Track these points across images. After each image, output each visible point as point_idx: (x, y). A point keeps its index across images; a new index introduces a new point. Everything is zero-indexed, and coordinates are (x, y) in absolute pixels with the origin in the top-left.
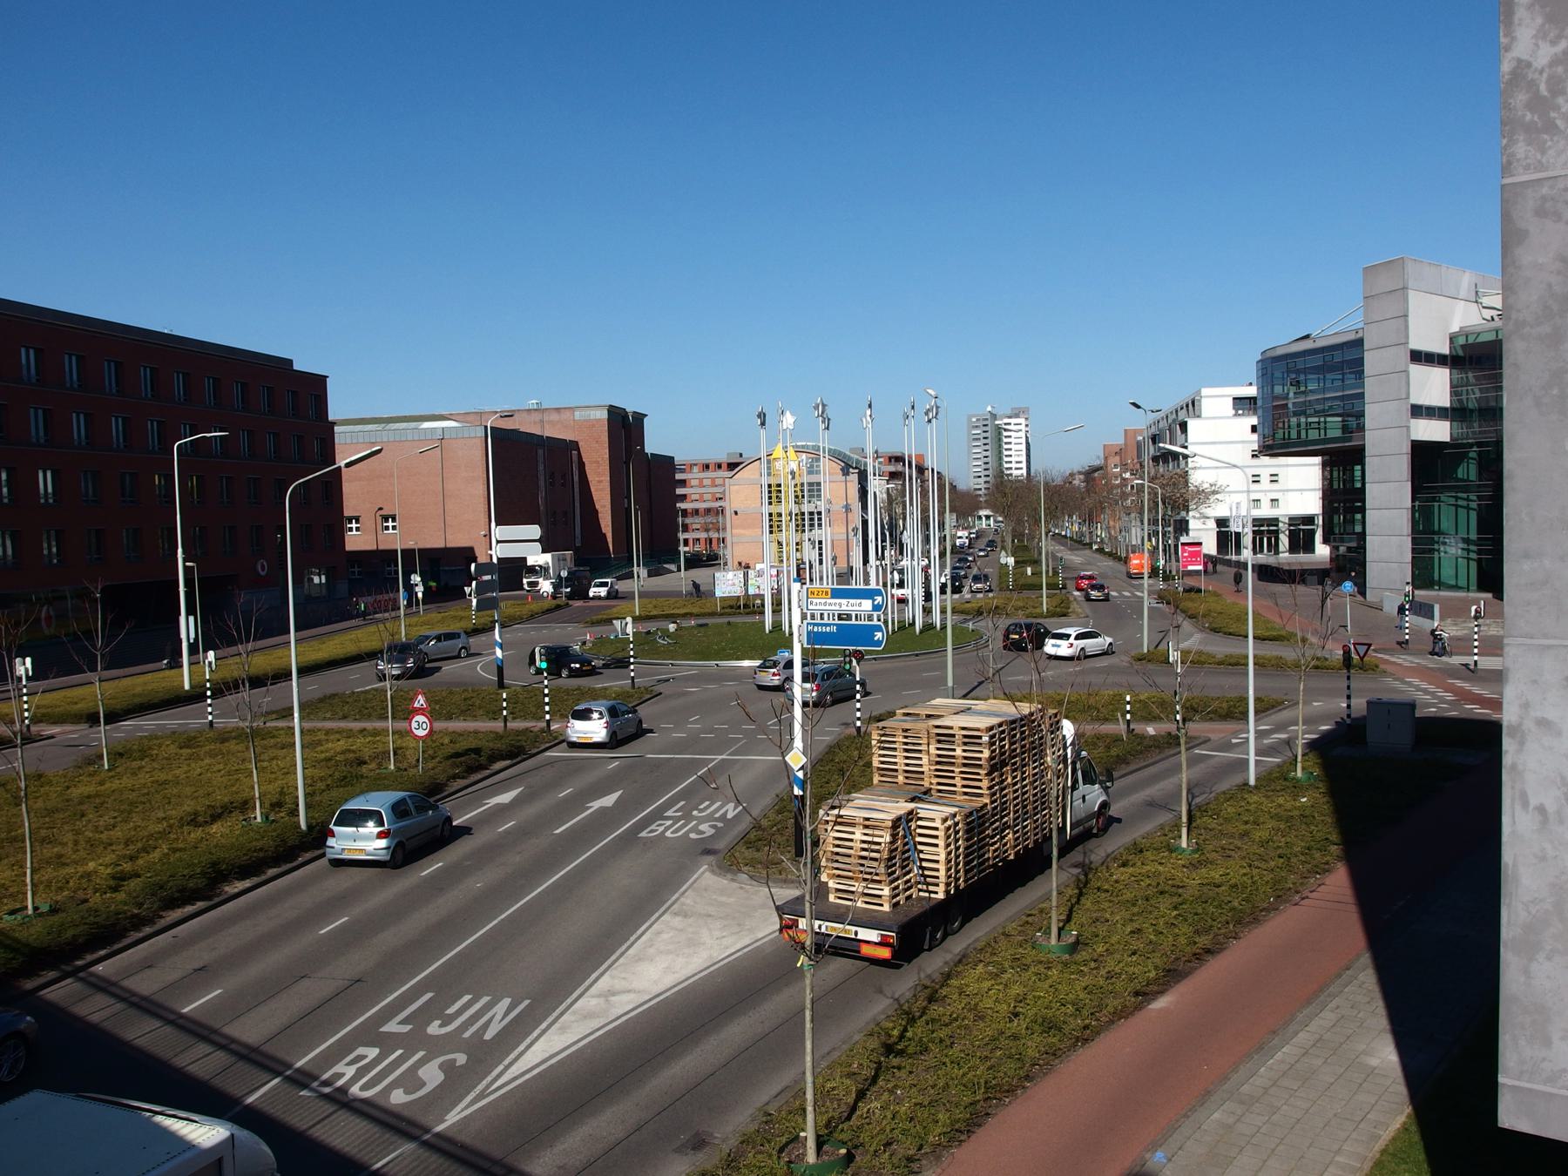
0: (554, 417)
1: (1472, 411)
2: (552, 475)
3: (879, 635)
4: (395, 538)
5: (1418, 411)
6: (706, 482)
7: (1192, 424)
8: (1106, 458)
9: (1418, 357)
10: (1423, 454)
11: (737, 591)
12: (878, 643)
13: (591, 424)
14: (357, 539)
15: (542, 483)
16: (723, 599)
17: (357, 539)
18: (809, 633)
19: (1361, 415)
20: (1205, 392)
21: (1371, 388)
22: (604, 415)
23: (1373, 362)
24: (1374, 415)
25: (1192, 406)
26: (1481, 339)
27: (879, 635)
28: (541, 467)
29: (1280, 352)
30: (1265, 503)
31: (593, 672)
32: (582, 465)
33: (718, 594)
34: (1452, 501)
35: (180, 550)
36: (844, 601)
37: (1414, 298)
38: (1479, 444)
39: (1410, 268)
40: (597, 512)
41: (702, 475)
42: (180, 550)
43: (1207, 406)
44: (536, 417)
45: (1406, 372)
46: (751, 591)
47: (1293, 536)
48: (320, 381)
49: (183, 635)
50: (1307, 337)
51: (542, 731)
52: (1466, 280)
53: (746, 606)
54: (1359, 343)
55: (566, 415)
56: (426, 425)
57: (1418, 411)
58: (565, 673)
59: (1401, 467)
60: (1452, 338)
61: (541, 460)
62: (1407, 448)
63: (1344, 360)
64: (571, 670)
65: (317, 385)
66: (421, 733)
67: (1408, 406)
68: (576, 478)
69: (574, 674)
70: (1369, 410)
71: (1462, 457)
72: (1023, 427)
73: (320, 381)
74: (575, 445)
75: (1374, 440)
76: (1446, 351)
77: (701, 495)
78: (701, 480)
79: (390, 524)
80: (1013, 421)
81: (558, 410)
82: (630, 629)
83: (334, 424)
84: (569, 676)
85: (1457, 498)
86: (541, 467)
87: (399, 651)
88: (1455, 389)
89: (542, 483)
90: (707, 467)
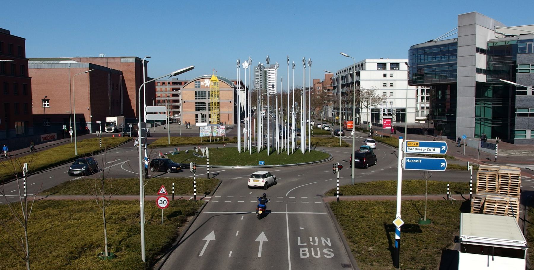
0: (112, 61)
1: (492, 71)
2: (113, 85)
3: (443, 164)
5: (479, 71)
6: (163, 89)
7: (362, 73)
9: (479, 50)
11: (209, 134)
12: (443, 168)
13: (128, 64)
14: (37, 109)
15: (110, 88)
16: (202, 137)
17: (37, 109)
18: (407, 163)
19: (456, 71)
20: (367, 61)
21: (460, 61)
23: (461, 51)
24: (461, 71)
25: (362, 66)
27: (443, 164)
28: (109, 81)
29: (421, 46)
30: (388, 104)
31: (180, 171)
32: (124, 81)
33: (201, 135)
34: (483, 105)
36: (426, 148)
37: (478, 28)
38: (494, 84)
39: (477, 16)
40: (130, 100)
43: (368, 66)
44: (105, 60)
46: (214, 135)
47: (398, 116)
48: (22, 41)
50: (432, 41)
52: (491, 22)
54: (455, 44)
55: (117, 60)
56: (62, 62)
57: (479, 71)
58: (169, 171)
59: (472, 91)
60: (488, 44)
61: (109, 78)
63: (449, 50)
64: (172, 169)
66: (163, 206)
68: (121, 86)
69: (173, 171)
71: (487, 88)
72: (274, 72)
73: (22, 41)
74: (121, 73)
78: (161, 89)
79: (46, 103)
81: (114, 58)
82: (207, 152)
84: (171, 172)
85: (485, 104)
86: (109, 81)
87: (76, 160)
89: (110, 88)
90: (164, 83)
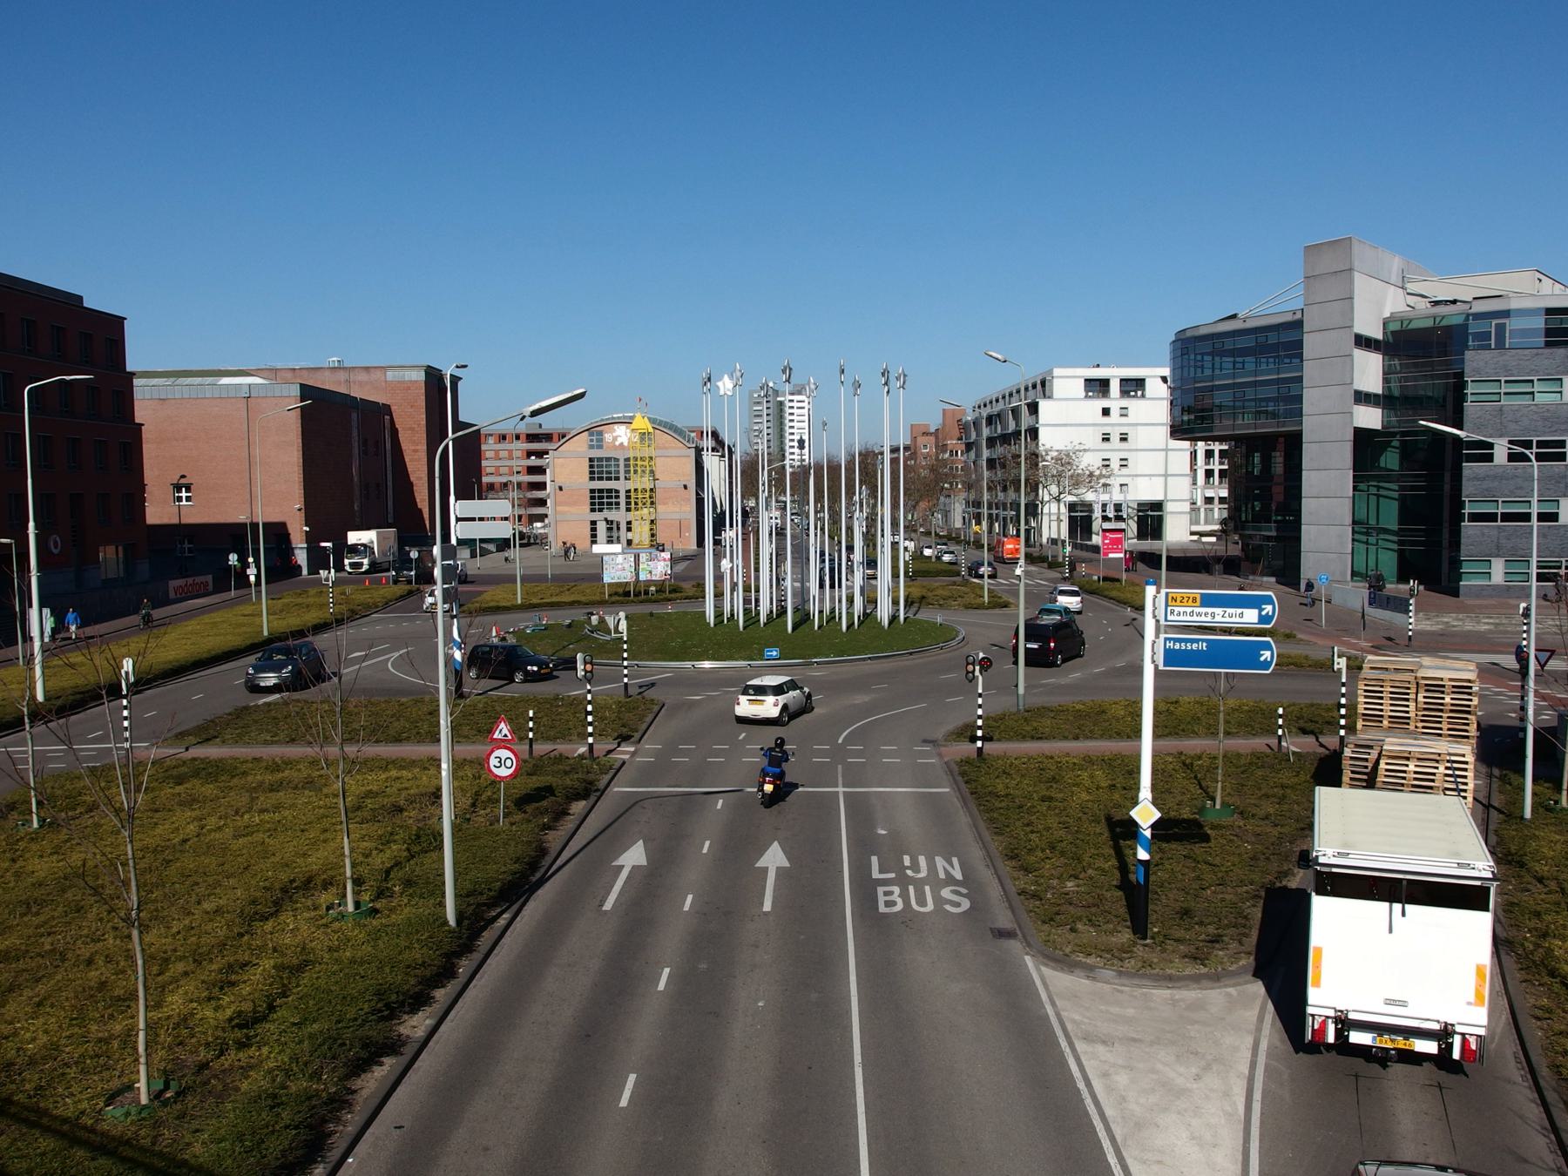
0: (363, 377)
4: (193, 511)
5: (1363, 398)
6: (503, 454)
7: (1044, 405)
8: (914, 439)
9: (1364, 342)
10: (1362, 437)
12: (1266, 665)
13: (407, 386)
14: (158, 512)
15: (356, 451)
17: (158, 512)
18: (1167, 652)
19: (1300, 399)
20: (1057, 372)
21: (1310, 371)
22: (421, 376)
24: (1311, 399)
25: (1043, 386)
26: (1413, 325)
27: (1266, 655)
28: (355, 433)
29: (1203, 331)
31: (549, 677)
32: (394, 432)
33: (607, 579)
35: (31, 524)
38: (1404, 434)
39: (1356, 247)
41: (499, 446)
42: (31, 524)
44: (342, 376)
45: (1351, 355)
46: (643, 577)
47: (1142, 522)
49: (35, 632)
50: (1234, 317)
51: (582, 757)
53: (637, 594)
54: (1298, 325)
55: (378, 375)
57: (1363, 398)
58: (519, 677)
61: (355, 424)
62: (1350, 436)
63: (1281, 343)
64: (527, 673)
65: (114, 325)
67: (1345, 393)
68: (388, 446)
69: (530, 678)
70: (1307, 395)
72: (805, 404)
73: (118, 322)
74: (387, 409)
75: (1311, 427)
76: (1380, 337)
77: (498, 468)
78: (497, 452)
79: (184, 494)
80: (796, 398)
81: (367, 369)
82: (623, 626)
83: (133, 374)
84: (525, 681)
85: (1379, 488)
86: (355, 433)
87: (266, 649)
88: (1387, 374)
89: (356, 451)
90: (504, 437)
